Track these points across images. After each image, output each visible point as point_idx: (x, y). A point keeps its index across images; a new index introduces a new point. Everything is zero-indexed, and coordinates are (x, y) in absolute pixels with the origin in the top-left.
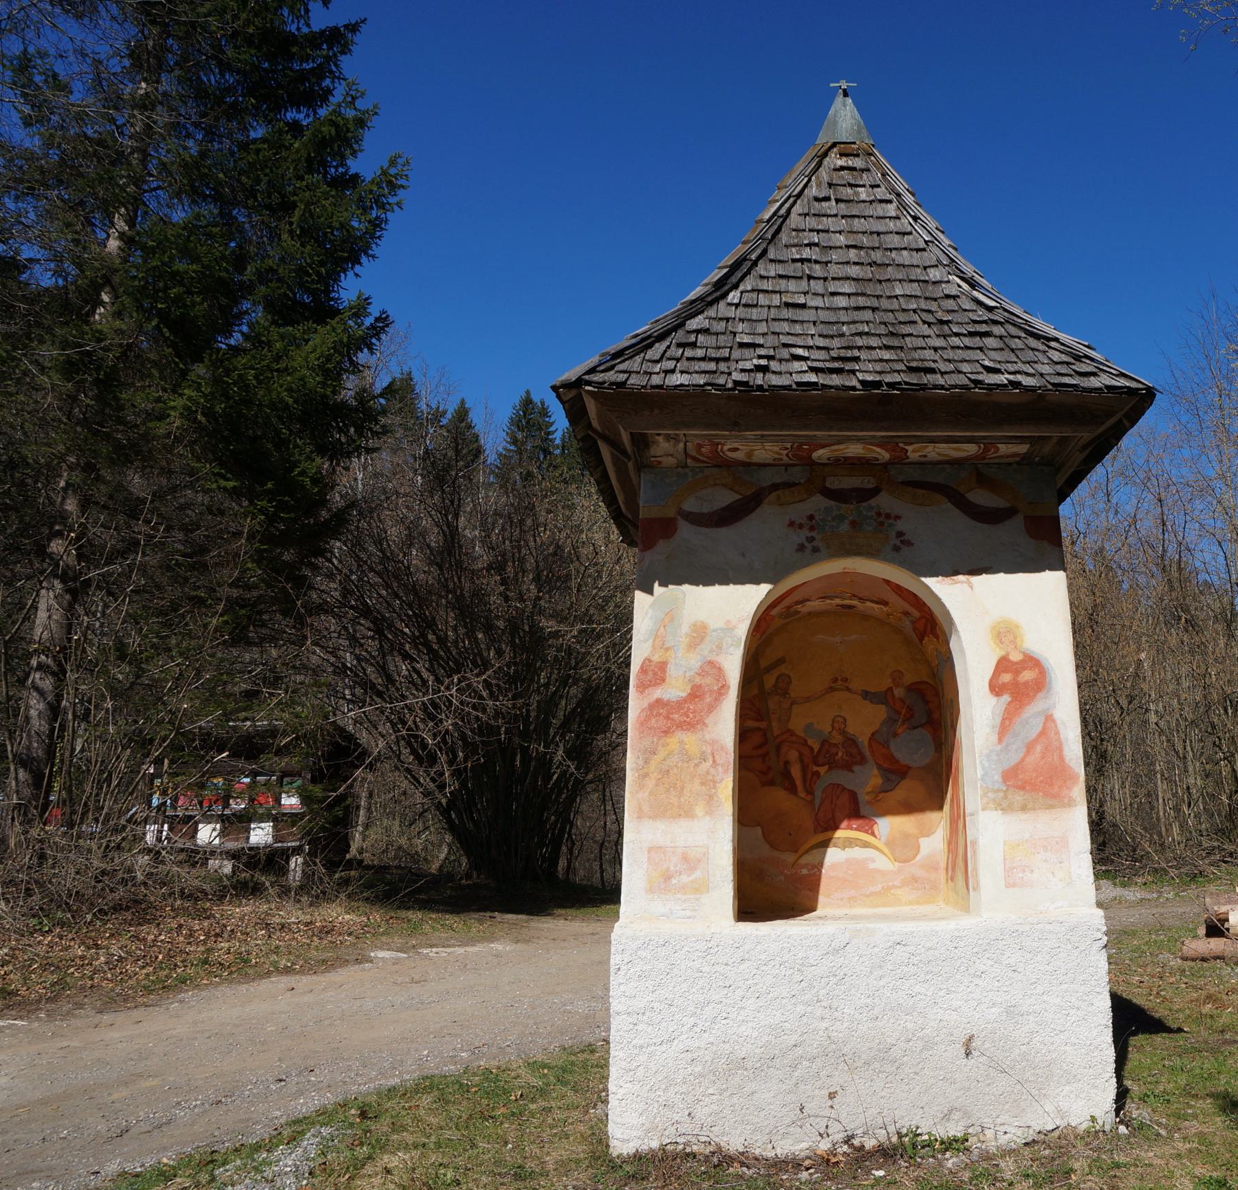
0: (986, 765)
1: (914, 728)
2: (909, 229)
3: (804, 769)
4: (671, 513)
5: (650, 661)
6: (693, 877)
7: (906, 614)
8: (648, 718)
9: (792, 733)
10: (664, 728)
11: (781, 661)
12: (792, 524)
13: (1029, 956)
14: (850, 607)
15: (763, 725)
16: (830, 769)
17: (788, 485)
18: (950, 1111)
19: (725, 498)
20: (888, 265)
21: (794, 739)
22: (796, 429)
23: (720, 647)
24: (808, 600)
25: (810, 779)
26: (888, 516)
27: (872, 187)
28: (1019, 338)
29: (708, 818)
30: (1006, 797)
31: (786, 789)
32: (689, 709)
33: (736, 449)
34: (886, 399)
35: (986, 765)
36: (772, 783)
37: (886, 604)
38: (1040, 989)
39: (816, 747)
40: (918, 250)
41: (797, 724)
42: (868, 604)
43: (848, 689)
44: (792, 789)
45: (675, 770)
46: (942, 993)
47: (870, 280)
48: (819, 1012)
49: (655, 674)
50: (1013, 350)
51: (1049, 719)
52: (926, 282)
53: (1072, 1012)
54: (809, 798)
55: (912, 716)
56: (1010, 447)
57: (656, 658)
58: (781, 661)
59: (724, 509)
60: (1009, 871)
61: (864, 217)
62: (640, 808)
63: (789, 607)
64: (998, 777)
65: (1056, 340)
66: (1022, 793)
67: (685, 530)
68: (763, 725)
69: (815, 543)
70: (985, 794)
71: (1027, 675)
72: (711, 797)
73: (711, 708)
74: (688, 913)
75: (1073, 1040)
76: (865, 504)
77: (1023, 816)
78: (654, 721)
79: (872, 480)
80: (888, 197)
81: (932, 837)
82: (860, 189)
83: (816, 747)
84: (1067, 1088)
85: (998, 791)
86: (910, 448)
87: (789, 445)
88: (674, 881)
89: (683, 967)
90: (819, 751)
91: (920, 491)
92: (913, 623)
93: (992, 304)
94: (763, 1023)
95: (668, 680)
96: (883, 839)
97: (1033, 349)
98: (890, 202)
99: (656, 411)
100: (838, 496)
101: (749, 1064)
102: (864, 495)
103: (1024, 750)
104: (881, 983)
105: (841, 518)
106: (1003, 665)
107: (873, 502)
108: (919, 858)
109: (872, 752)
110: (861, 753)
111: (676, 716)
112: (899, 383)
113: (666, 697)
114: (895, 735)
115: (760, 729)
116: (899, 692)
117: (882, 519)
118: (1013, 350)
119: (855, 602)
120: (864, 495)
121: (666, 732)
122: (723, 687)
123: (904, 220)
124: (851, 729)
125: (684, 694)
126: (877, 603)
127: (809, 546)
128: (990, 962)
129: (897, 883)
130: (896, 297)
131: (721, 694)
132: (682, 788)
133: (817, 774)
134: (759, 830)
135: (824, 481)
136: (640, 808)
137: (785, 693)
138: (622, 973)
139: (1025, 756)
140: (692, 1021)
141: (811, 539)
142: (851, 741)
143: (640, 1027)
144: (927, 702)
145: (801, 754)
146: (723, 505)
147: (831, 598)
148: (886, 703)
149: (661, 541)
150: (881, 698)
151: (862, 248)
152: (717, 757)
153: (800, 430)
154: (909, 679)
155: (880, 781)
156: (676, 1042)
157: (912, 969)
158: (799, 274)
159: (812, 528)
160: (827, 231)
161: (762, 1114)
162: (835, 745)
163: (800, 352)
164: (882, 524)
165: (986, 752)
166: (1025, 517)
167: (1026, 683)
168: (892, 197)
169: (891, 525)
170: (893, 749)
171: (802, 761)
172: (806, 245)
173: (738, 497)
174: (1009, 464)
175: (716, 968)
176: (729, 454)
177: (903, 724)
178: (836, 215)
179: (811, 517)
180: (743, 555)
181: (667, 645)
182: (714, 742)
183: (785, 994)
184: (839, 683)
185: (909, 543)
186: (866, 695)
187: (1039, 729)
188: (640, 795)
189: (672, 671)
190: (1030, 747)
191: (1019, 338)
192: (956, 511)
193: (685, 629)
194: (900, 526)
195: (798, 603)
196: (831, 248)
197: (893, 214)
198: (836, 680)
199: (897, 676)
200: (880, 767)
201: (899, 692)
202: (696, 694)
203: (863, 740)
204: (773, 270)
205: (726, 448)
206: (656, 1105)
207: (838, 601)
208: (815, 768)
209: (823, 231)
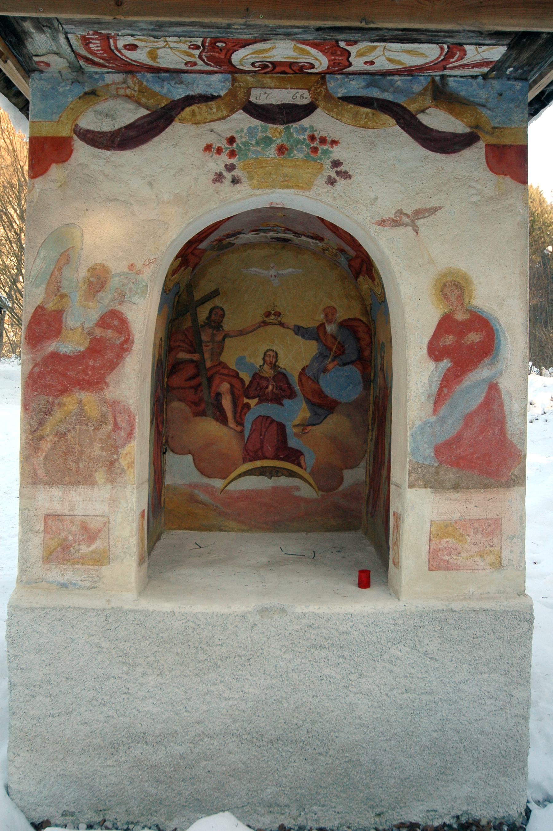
0: (418, 438)
1: (344, 365)
3: (235, 402)
4: (65, 131)
7: (342, 251)
9: (225, 367)
11: (215, 294)
12: (208, 148)
14: (285, 240)
15: (196, 357)
16: (260, 402)
19: (128, 114)
21: (225, 372)
23: (122, 295)
24: (239, 233)
25: (240, 410)
26: (323, 141)
29: (109, 486)
31: (217, 420)
33: (133, 47)
36: (202, 414)
37: (321, 239)
39: (247, 379)
41: (230, 358)
42: (303, 238)
43: (281, 324)
44: (223, 420)
54: (239, 428)
55: (343, 353)
57: (50, 306)
58: (215, 294)
59: (127, 127)
60: (433, 554)
63: (220, 240)
64: (430, 452)
66: (454, 470)
67: (82, 151)
68: (196, 357)
69: (235, 173)
71: (474, 337)
72: (112, 463)
73: (112, 366)
76: (295, 125)
77: (454, 495)
83: (247, 379)
86: (353, 50)
87: (199, 42)
90: (251, 382)
92: (349, 260)
95: (64, 332)
96: (309, 470)
101: (150, 739)
102: (291, 114)
103: (462, 423)
105: (267, 141)
106: (446, 324)
107: (306, 122)
108: (341, 488)
110: (290, 388)
114: (325, 370)
115: (192, 361)
117: (316, 144)
119: (289, 236)
120: (291, 114)
121: (64, 391)
122: (126, 341)
126: (312, 238)
127: (228, 176)
133: (248, 406)
134: (190, 457)
137: (218, 327)
141: (230, 168)
142: (281, 377)
144: (358, 339)
145: (232, 386)
146: (128, 122)
147: (265, 231)
148: (318, 339)
149: (54, 166)
150: (314, 334)
154: (342, 315)
155: (308, 414)
159: (232, 154)
164: (315, 150)
166: (487, 146)
169: (325, 152)
170: (322, 383)
171: (233, 393)
173: (144, 112)
174: (475, 77)
176: (128, 53)
177: (333, 360)
179: (231, 140)
180: (150, 184)
182: (114, 403)
184: (273, 317)
185: (346, 175)
186: (299, 330)
187: (481, 399)
189: (71, 321)
190: (469, 419)
192: (405, 135)
193: (83, 273)
194: (337, 153)
195: (228, 236)
198: (268, 314)
199: (330, 312)
200: (309, 402)
201: (330, 328)
202: (96, 348)
203: (294, 379)
205: (121, 43)
207: (272, 234)
208: (246, 400)
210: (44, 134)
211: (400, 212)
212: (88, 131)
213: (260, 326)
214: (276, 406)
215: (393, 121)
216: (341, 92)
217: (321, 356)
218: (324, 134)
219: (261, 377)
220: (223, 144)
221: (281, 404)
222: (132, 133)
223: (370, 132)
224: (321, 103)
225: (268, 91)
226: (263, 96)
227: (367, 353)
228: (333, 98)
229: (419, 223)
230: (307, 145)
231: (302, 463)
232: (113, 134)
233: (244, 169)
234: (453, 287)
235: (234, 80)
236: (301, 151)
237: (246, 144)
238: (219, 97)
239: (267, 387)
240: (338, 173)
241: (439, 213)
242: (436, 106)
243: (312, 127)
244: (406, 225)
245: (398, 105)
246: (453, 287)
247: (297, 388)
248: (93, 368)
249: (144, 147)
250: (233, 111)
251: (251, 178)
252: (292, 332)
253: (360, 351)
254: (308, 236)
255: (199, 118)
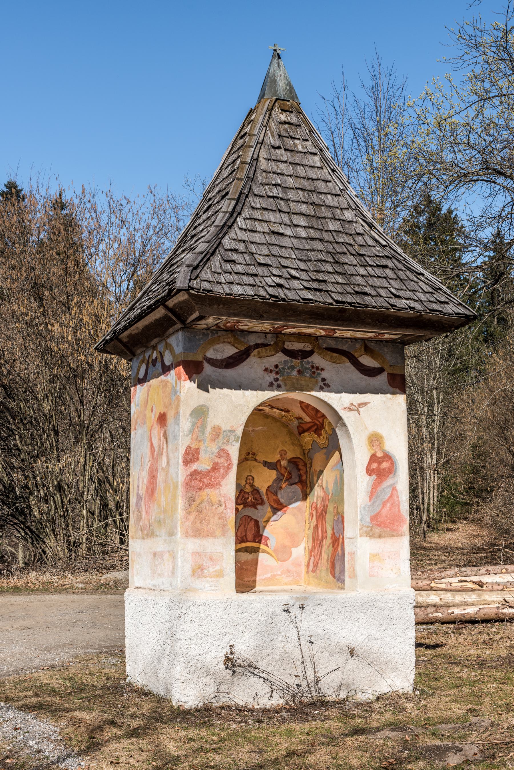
0: (363, 513)
1: (292, 485)
2: (330, 178)
4: (200, 358)
5: (190, 447)
6: (216, 569)
8: (190, 480)
10: (199, 487)
12: (266, 370)
13: (380, 611)
16: (245, 507)
17: (264, 345)
18: (341, 685)
19: (229, 351)
20: (322, 205)
22: (292, 322)
26: (317, 368)
27: (304, 140)
28: (402, 270)
29: (222, 538)
30: (371, 530)
32: (212, 476)
34: (344, 310)
35: (363, 513)
38: (384, 627)
40: (337, 195)
43: (256, 460)
45: (205, 511)
46: (338, 629)
47: (313, 216)
48: (280, 638)
49: (193, 455)
50: (401, 280)
51: (394, 489)
52: (344, 220)
53: (398, 638)
55: (291, 477)
56: (389, 335)
57: (193, 446)
59: (230, 358)
61: (303, 165)
62: (187, 531)
64: (368, 520)
65: (423, 275)
66: (379, 528)
69: (279, 382)
70: (361, 529)
73: (224, 476)
74: (213, 588)
75: (398, 651)
76: (305, 360)
78: (193, 482)
79: (310, 346)
80: (314, 150)
81: (299, 547)
82: (298, 142)
84: (394, 674)
85: (368, 527)
88: (206, 571)
89: (213, 616)
91: (335, 355)
93: (384, 243)
94: (253, 644)
95: (200, 459)
96: (272, 548)
97: (412, 281)
98: (316, 154)
99: (221, 306)
100: (291, 354)
102: (305, 354)
103: (382, 506)
104: (310, 624)
105: (292, 368)
106: (373, 458)
107: (310, 359)
108: (291, 559)
109: (268, 498)
110: (261, 498)
111: (205, 480)
112: (354, 303)
113: (199, 469)
114: (281, 488)
116: (284, 463)
117: (314, 370)
118: (401, 280)
122: (230, 464)
123: (325, 170)
124: (256, 484)
125: (209, 468)
128: (362, 614)
129: (279, 573)
130: (330, 231)
131: (229, 469)
132: (209, 521)
135: (284, 344)
136: (187, 531)
138: (182, 619)
139: (382, 509)
140: (217, 643)
141: (276, 380)
142: (256, 491)
143: (192, 646)
146: (229, 355)
148: (276, 469)
151: (305, 190)
152: (227, 504)
153: (294, 322)
154: (290, 455)
156: (210, 654)
157: (325, 617)
158: (274, 209)
159: (277, 373)
160: (283, 174)
161: (252, 688)
162: (248, 493)
163: (293, 272)
164: (314, 373)
165: (363, 506)
167: (384, 469)
168: (316, 151)
170: (279, 496)
172: (274, 185)
175: (230, 616)
178: (286, 162)
179: (276, 366)
181: (199, 439)
182: (225, 496)
183: (264, 629)
184: (251, 456)
186: (266, 464)
187: (389, 494)
188: (187, 524)
189: (202, 455)
191: (402, 270)
194: (324, 375)
196: (287, 188)
197: (318, 164)
198: (248, 454)
201: (284, 463)
202: (215, 468)
203: (263, 490)
204: (257, 203)
206: (201, 684)
209: (281, 174)
210: (190, 359)
211: (352, 404)
212: (211, 359)
213: (244, 461)
214: (253, 509)
215: (347, 360)
216: (325, 346)
217: (278, 480)
218: (318, 365)
219: (245, 492)
220: (273, 368)
221: (257, 509)
222: (231, 361)
223: (338, 365)
224: (316, 350)
225: (293, 343)
226: (290, 346)
227: (304, 478)
228: (321, 348)
229: (360, 409)
230: (311, 370)
231: (269, 544)
232: (222, 361)
233: (282, 380)
234: (375, 439)
235: (277, 337)
236: (308, 373)
237: (283, 368)
238: (270, 345)
239: (248, 498)
240: (324, 384)
241: (368, 405)
242: (366, 354)
243: (312, 362)
244: (355, 410)
245: (349, 353)
246: (375, 439)
247: (265, 498)
248: (215, 478)
249: (237, 367)
250: (277, 352)
251: (286, 385)
252: (262, 465)
253: (300, 476)
254: (278, 409)
255: (261, 354)
